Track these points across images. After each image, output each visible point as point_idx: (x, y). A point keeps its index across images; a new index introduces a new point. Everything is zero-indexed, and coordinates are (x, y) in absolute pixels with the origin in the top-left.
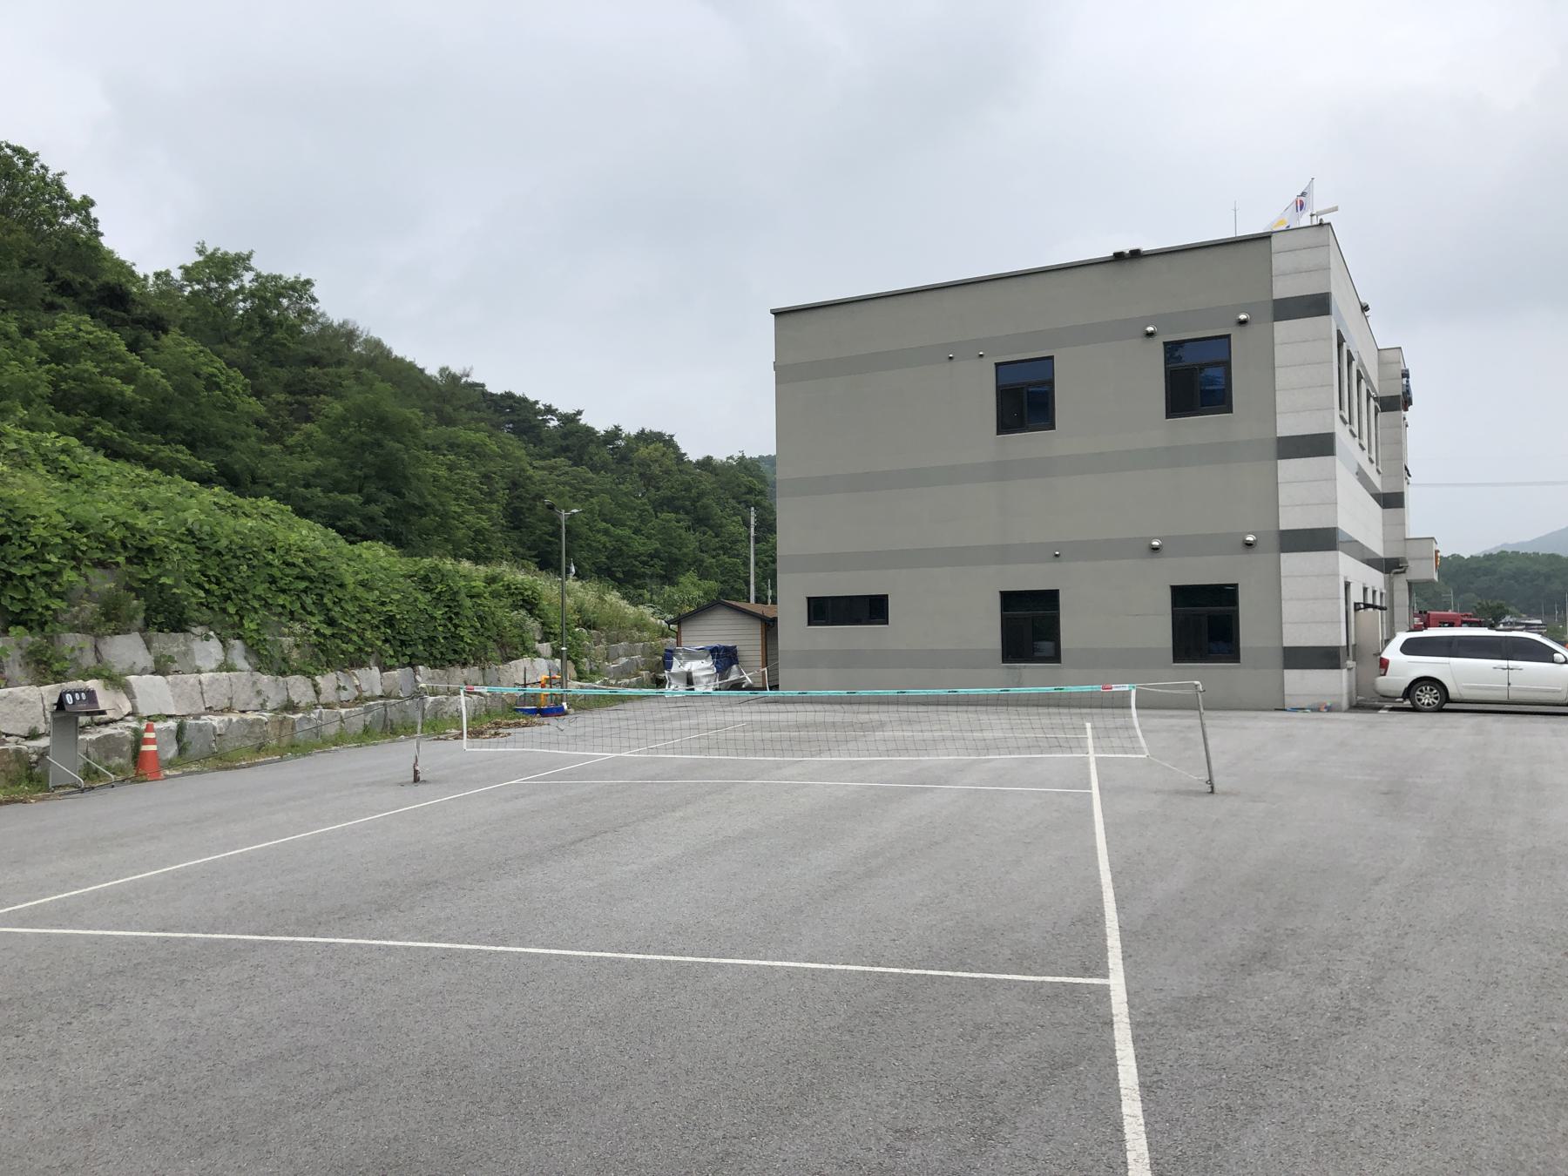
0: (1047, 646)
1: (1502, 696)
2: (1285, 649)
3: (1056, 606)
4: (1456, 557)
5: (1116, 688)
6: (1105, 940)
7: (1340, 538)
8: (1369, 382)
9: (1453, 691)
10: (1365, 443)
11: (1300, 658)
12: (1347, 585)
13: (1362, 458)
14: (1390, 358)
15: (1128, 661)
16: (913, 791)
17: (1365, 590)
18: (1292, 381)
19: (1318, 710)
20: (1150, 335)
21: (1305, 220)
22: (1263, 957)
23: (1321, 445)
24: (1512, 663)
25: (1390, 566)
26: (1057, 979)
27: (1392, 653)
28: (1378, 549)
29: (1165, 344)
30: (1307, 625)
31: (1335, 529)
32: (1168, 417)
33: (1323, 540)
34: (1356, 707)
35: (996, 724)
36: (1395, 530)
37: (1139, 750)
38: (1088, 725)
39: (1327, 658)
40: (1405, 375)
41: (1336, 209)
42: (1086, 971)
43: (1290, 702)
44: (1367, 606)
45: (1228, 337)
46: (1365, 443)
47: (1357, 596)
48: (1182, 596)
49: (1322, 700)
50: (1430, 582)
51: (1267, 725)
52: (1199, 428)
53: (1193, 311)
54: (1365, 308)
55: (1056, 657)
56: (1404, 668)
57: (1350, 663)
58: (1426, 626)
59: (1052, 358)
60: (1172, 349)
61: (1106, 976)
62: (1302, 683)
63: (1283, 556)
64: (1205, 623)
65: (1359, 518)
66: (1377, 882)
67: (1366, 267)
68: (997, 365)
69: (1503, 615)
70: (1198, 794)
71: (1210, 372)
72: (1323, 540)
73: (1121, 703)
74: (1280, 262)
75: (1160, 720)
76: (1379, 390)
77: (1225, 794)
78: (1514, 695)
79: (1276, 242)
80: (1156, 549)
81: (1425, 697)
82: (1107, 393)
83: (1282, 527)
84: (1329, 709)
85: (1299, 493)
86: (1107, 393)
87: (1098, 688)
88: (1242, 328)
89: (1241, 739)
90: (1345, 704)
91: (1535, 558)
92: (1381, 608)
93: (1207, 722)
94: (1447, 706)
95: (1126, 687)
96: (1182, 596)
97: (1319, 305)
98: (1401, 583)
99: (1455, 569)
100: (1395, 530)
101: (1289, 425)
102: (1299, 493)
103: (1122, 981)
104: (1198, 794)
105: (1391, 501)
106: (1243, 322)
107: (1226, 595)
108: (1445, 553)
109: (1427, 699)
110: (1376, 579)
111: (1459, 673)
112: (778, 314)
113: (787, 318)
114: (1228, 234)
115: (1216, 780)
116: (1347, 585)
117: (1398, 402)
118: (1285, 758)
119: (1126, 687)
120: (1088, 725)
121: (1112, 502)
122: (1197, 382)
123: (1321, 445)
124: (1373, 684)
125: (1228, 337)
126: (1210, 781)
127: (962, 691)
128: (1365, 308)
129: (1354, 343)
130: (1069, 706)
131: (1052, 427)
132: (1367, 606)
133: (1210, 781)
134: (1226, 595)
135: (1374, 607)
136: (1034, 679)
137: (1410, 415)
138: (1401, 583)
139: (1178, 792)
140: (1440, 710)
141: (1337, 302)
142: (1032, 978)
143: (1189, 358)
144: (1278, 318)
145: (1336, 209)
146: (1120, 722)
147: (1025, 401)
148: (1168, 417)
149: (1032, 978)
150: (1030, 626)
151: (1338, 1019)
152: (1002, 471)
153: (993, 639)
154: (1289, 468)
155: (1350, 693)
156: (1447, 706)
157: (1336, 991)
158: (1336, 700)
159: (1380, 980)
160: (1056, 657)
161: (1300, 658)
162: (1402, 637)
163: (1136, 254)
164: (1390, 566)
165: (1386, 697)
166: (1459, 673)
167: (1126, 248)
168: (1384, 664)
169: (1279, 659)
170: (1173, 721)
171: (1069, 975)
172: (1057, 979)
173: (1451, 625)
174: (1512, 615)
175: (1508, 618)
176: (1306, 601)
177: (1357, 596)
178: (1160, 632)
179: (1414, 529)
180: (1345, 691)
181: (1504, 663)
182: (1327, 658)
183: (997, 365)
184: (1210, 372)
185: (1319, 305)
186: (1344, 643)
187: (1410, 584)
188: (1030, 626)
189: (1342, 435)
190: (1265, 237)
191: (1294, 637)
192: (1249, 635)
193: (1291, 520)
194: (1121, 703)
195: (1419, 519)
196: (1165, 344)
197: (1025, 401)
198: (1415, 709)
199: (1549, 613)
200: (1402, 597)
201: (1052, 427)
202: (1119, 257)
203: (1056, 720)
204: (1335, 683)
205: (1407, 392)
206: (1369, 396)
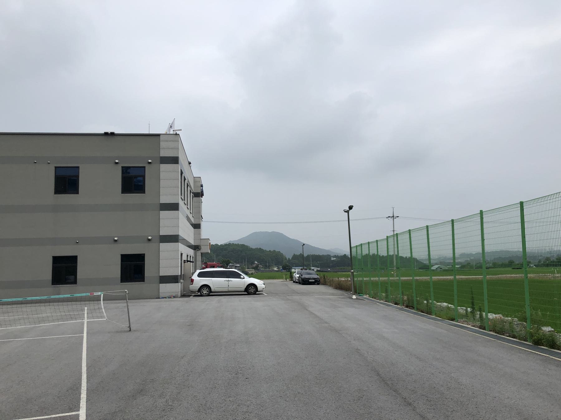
0: (72, 277)
1: (226, 290)
2: (160, 277)
3: (76, 262)
4: (217, 245)
5: (95, 294)
6: (80, 395)
7: (180, 238)
8: (191, 187)
9: (213, 289)
10: (189, 207)
11: (166, 279)
12: (182, 254)
13: (188, 212)
14: (197, 180)
15: (102, 283)
16: (4, 342)
17: (187, 256)
18: (165, 184)
19: (171, 298)
20: (117, 163)
21: (172, 132)
22: (141, 392)
23: (174, 207)
24: (229, 279)
25: (196, 248)
26: (57, 415)
27: (195, 277)
28: (192, 242)
29: (122, 167)
30: (169, 268)
31: (178, 235)
32: (122, 193)
33: (174, 239)
34: (183, 296)
35: (46, 311)
36: (197, 236)
37: (102, 317)
38: (86, 308)
39: (174, 279)
40: (202, 186)
41: (181, 130)
42: (71, 410)
43: (161, 295)
44: (188, 261)
45: (144, 167)
46: (189, 207)
47: (184, 258)
48: (125, 258)
49: (172, 294)
50: (208, 253)
51: (152, 304)
52: (134, 198)
53: (134, 157)
54: (190, 163)
55: (75, 282)
56: (199, 281)
57: (182, 281)
58: (207, 267)
59: (78, 167)
60: (125, 170)
61: (79, 410)
62: (166, 288)
63: (161, 244)
64: (133, 268)
65: (186, 232)
66: (182, 358)
67: (190, 148)
68: (56, 167)
69: (229, 263)
70: (125, 332)
71: (139, 178)
72: (174, 239)
73: (98, 299)
74: (163, 144)
75: (113, 305)
76: (194, 190)
77: (134, 331)
78: (230, 289)
79: (162, 138)
80: (116, 241)
81: (205, 291)
82: (100, 182)
83: (162, 233)
84: (174, 297)
85: (168, 223)
86: (100, 182)
87: (88, 294)
88: (150, 165)
89: (144, 311)
90: (179, 295)
91: (238, 245)
92: (192, 262)
93: (129, 304)
94: (211, 294)
95: (99, 293)
96: (125, 258)
97: (175, 160)
98: (199, 253)
99: (216, 249)
100: (197, 236)
101: (165, 199)
102: (168, 223)
103: (85, 411)
104: (125, 332)
105: (197, 226)
106: (150, 163)
107: (141, 258)
108: (213, 243)
109: (205, 292)
110: (191, 252)
111: (215, 283)
114: (146, 132)
115: (132, 326)
116: (182, 254)
117: (199, 194)
118: (158, 315)
119: (99, 293)
120: (86, 308)
121: (97, 225)
122: (133, 182)
123: (174, 207)
125: (144, 167)
126: (130, 327)
127: (29, 298)
128: (190, 163)
129: (186, 174)
130: (76, 301)
131: (78, 193)
132: (188, 261)
133: (130, 327)
134: (141, 258)
135: (190, 261)
136: (65, 291)
137: (203, 199)
138: (199, 253)
139: (117, 332)
140: (209, 295)
141: (181, 159)
142: (46, 417)
143: (132, 173)
144: (161, 163)
145: (181, 130)
146: (96, 307)
147: (67, 182)
148: (122, 193)
149: (46, 417)
151: (164, 410)
153: (48, 276)
154: (164, 214)
155: (181, 291)
156: (211, 294)
157: (164, 400)
159: (179, 393)
160: (75, 282)
161: (166, 279)
162: (198, 271)
163: (112, 134)
164: (196, 248)
165: (192, 292)
166: (215, 283)
167: (109, 131)
168: (192, 281)
169: (158, 280)
170: (118, 305)
171: (62, 413)
172: (57, 415)
173: (214, 267)
174: (232, 263)
175: (230, 264)
176: (168, 260)
177: (184, 258)
178: (116, 271)
179: (203, 236)
180: (180, 290)
181: (227, 279)
182: (174, 279)
183: (56, 167)
184: (139, 178)
185: (175, 160)
186: (180, 274)
187: (202, 253)
188: (64, 270)
189: (181, 203)
190: (158, 135)
191: (164, 272)
192: (149, 272)
193: (164, 232)
194: (98, 299)
195: (205, 233)
196: (122, 167)
197: (67, 182)
198: (201, 296)
199: (242, 262)
200: (199, 258)
201: (78, 193)
202: (106, 134)
203: (74, 306)
204: (176, 288)
205: (202, 192)
206: (190, 192)
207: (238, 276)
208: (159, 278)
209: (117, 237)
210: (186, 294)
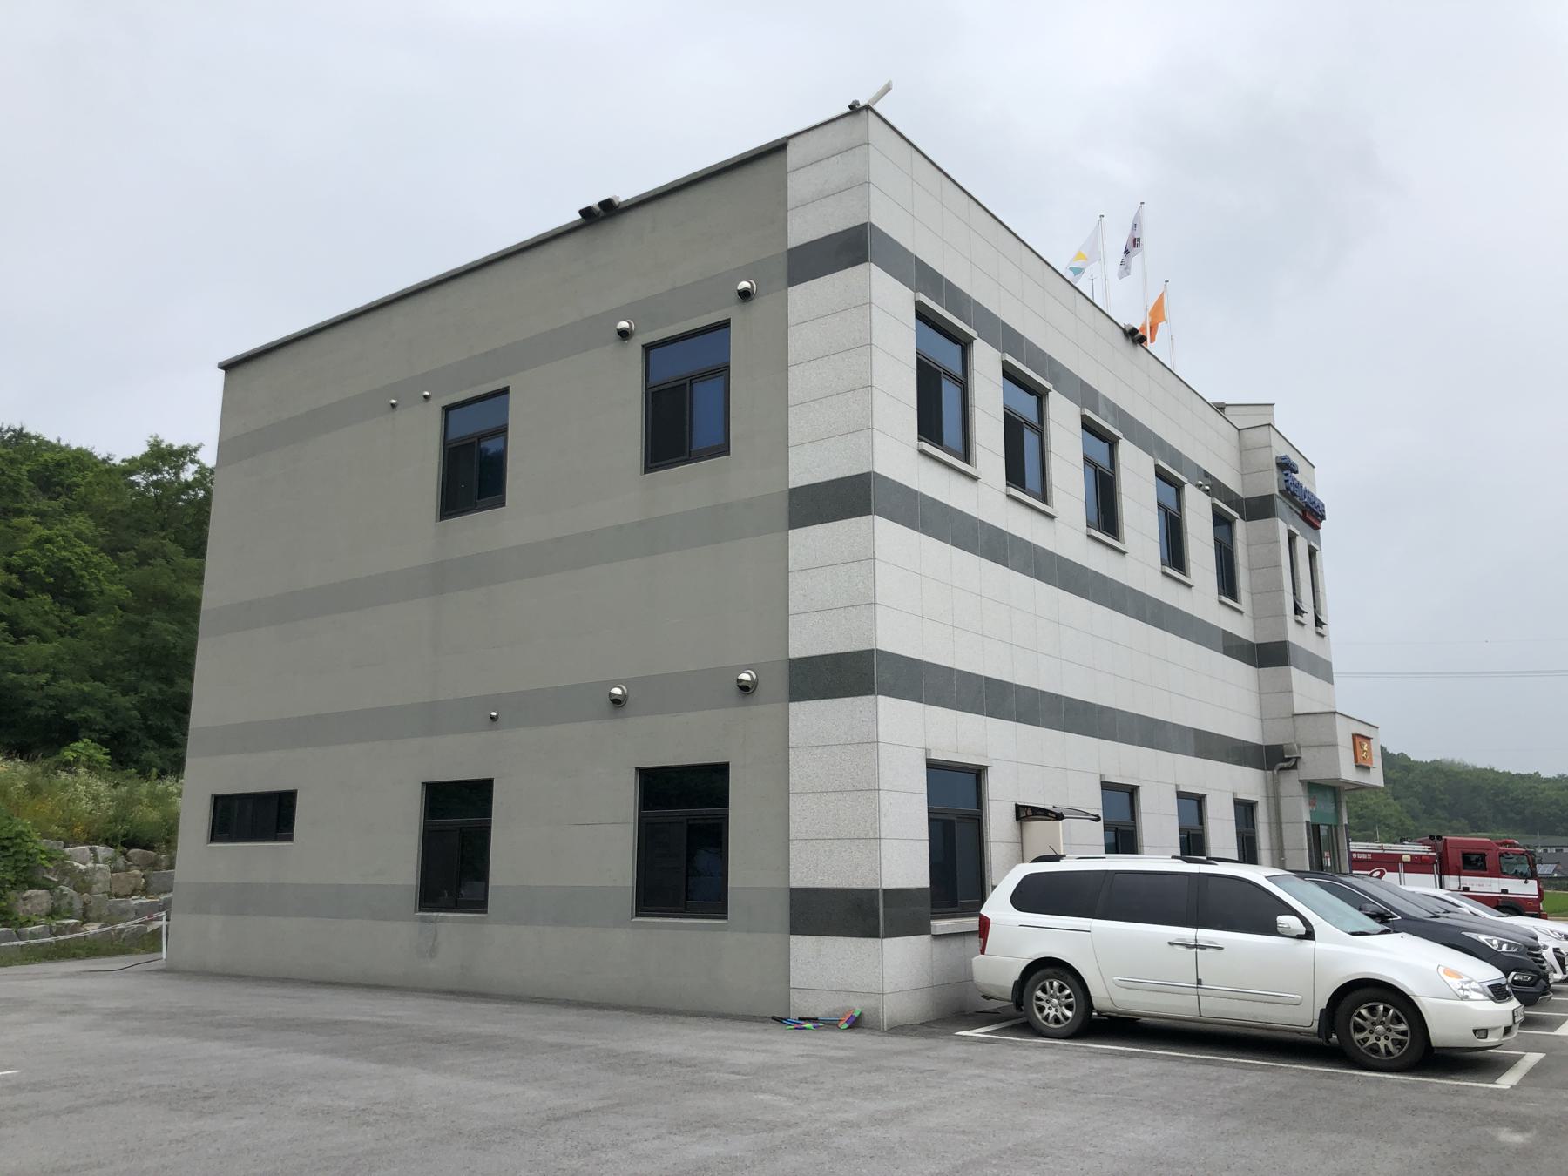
2: (794, 891)
14: (1248, 424)
20: (624, 334)
24: (1205, 935)
25: (1272, 758)
28: (1248, 731)
36: (1273, 703)
53: (654, 284)
62: (828, 966)
63: (794, 706)
64: (684, 836)
74: (799, 185)
98: (1291, 785)
106: (745, 295)
110: (1248, 782)
112: (229, 367)
113: (238, 373)
124: (968, 979)
144: (794, 280)
150: (456, 840)
152: (440, 578)
154: (808, 542)
158: (869, 1003)
163: (608, 207)
164: (1272, 758)
167: (593, 201)
169: (782, 913)
188: (456, 840)
191: (815, 869)
192: (745, 868)
204: (897, 966)
207: (1258, 913)
208: (784, 901)
209: (626, 682)
210: (958, 1010)
